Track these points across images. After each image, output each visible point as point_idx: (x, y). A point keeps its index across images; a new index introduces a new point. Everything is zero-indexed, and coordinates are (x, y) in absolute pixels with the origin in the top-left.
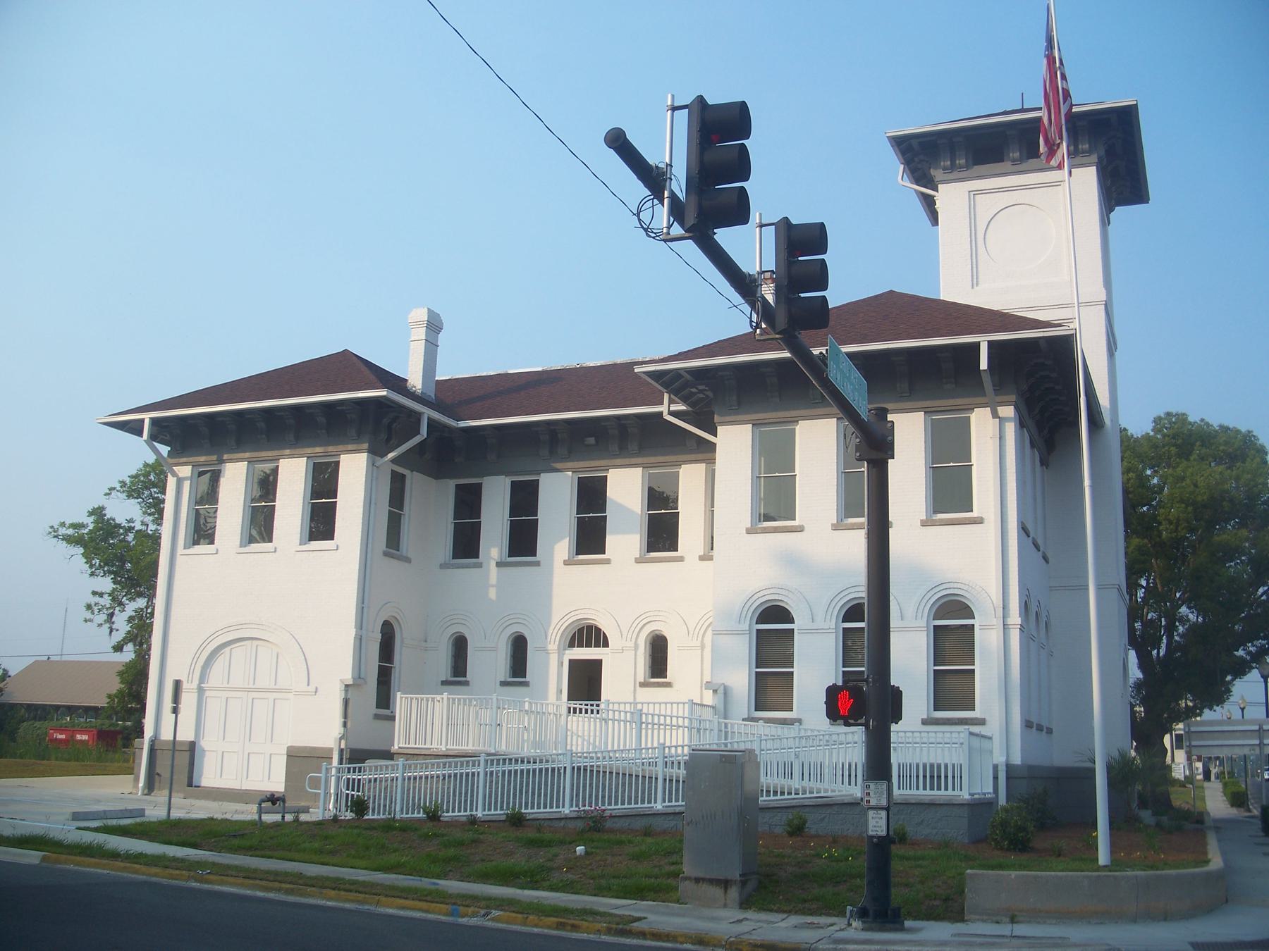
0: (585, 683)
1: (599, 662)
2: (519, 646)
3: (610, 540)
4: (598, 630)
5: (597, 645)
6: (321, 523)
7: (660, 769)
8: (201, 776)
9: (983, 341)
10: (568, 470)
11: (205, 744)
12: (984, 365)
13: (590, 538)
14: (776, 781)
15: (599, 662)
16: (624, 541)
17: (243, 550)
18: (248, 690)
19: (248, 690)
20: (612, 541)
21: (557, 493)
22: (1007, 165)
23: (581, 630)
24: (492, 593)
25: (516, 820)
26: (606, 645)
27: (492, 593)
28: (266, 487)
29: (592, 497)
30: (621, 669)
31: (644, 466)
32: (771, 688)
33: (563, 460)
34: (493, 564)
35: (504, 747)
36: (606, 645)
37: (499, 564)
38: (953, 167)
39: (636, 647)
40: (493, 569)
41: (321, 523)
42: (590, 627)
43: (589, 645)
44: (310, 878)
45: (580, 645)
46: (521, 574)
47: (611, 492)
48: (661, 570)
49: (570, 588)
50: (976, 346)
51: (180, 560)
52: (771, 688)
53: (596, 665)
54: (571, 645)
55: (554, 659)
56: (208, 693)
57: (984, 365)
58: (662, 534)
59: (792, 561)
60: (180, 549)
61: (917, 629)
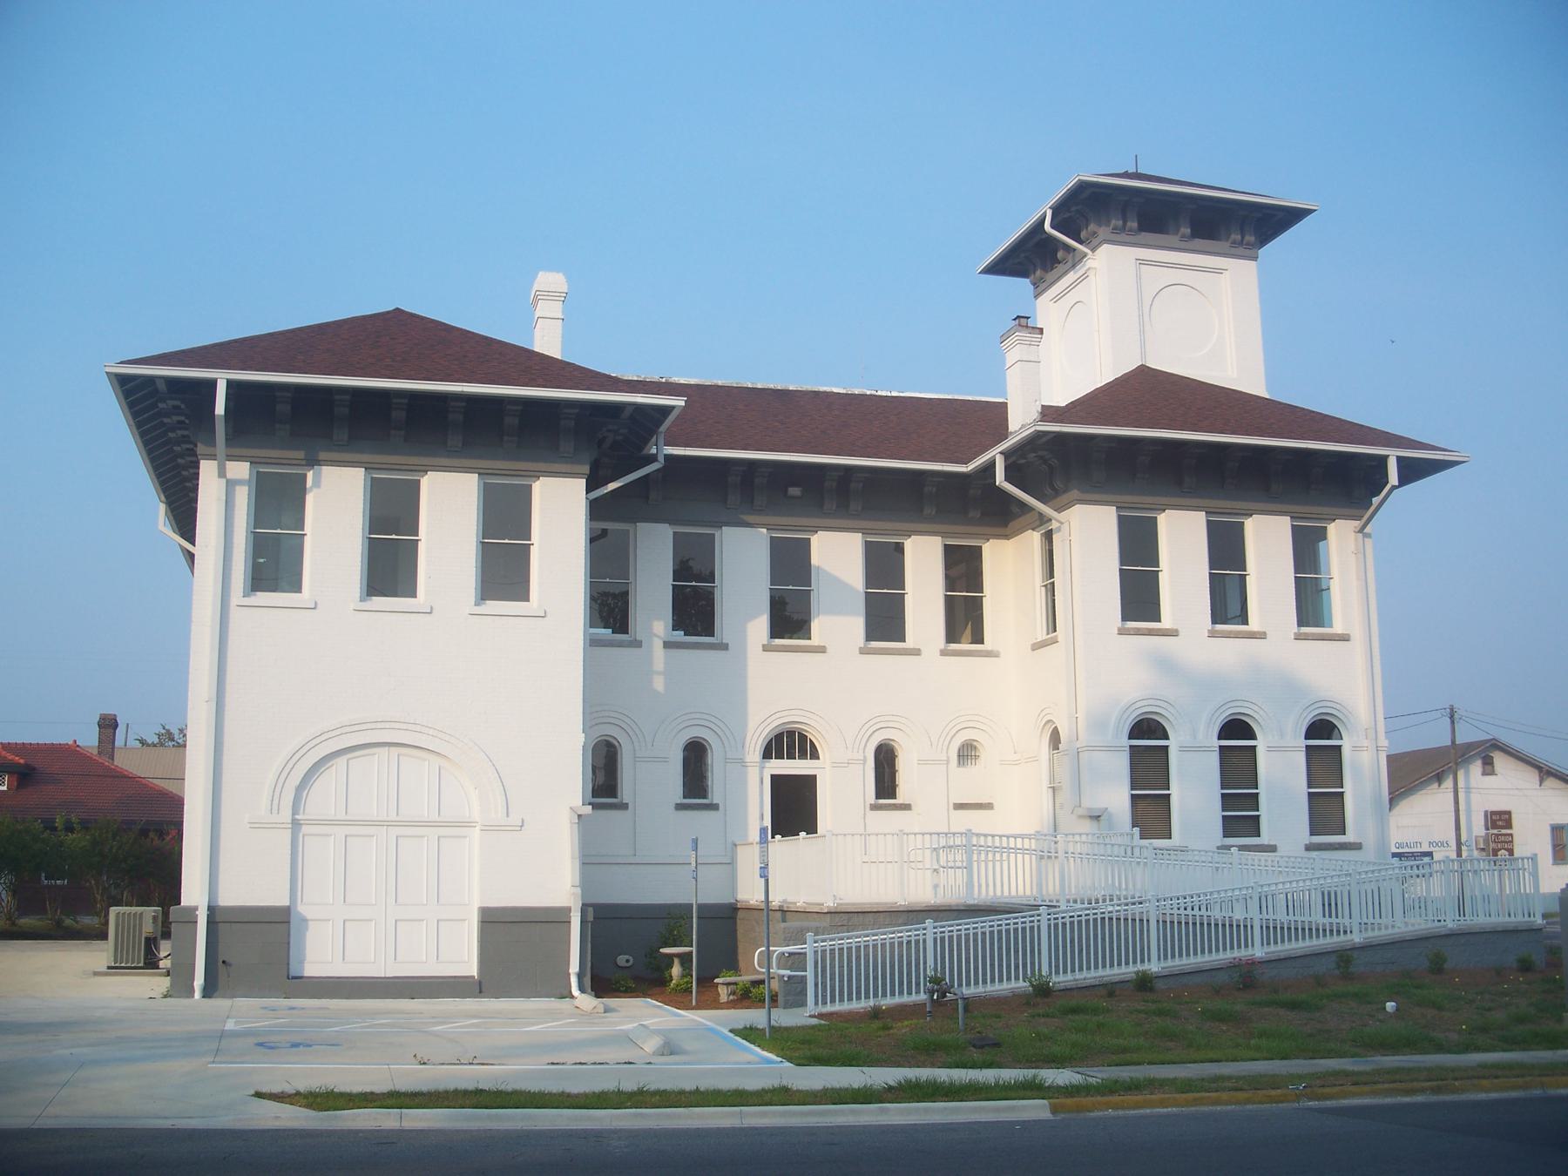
0: (794, 808)
1: (811, 780)
2: (695, 757)
3: (816, 625)
4: (803, 738)
5: (803, 756)
6: (504, 572)
7: (1254, 913)
8: (302, 962)
9: (221, 378)
10: (762, 526)
11: (302, 909)
12: (220, 409)
13: (789, 620)
14: (1306, 919)
15: (811, 780)
16: (838, 625)
17: (479, 610)
18: (389, 824)
19: (389, 824)
20: (820, 626)
21: (743, 558)
22: (1173, 239)
23: (779, 737)
24: (659, 684)
25: (1043, 991)
26: (815, 755)
27: (659, 684)
29: (791, 566)
30: (841, 786)
31: (864, 532)
32: (1152, 813)
33: (760, 512)
34: (658, 645)
35: (1006, 893)
36: (815, 755)
37: (668, 645)
38: (1123, 229)
39: (865, 760)
40: (658, 651)
41: (504, 572)
42: (791, 733)
43: (791, 756)
44: (577, 1096)
45: (780, 756)
46: (698, 660)
47: (816, 559)
48: (885, 665)
49: (770, 683)
50: (212, 384)
51: (236, 615)
52: (1152, 813)
53: (809, 782)
54: (767, 755)
55: (753, 775)
56: (305, 829)
57: (220, 409)
58: (964, 619)
59: (1166, 666)
61: (1294, 749)
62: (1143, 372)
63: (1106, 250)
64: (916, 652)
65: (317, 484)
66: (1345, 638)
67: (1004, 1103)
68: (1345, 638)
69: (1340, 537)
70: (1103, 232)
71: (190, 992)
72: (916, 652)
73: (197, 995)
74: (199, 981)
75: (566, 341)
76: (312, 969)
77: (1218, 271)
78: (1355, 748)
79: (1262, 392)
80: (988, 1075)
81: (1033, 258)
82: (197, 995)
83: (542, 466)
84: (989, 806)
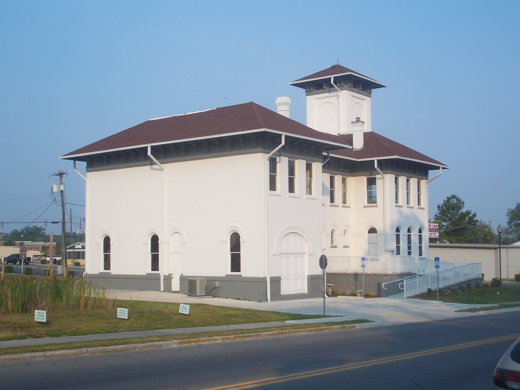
62: (252, 103)
63: (346, 91)
64: (349, 207)
65: (280, 161)
66: (423, 209)
67: (481, 311)
68: (423, 209)
69: (423, 182)
70: (346, 86)
71: (267, 300)
72: (349, 207)
73: (269, 301)
74: (269, 297)
75: (290, 115)
76: (282, 293)
77: (364, 100)
78: (425, 235)
79: (286, 115)
80: (511, 303)
81: (316, 85)
82: (269, 301)
83: (413, 175)
84: (155, 240)
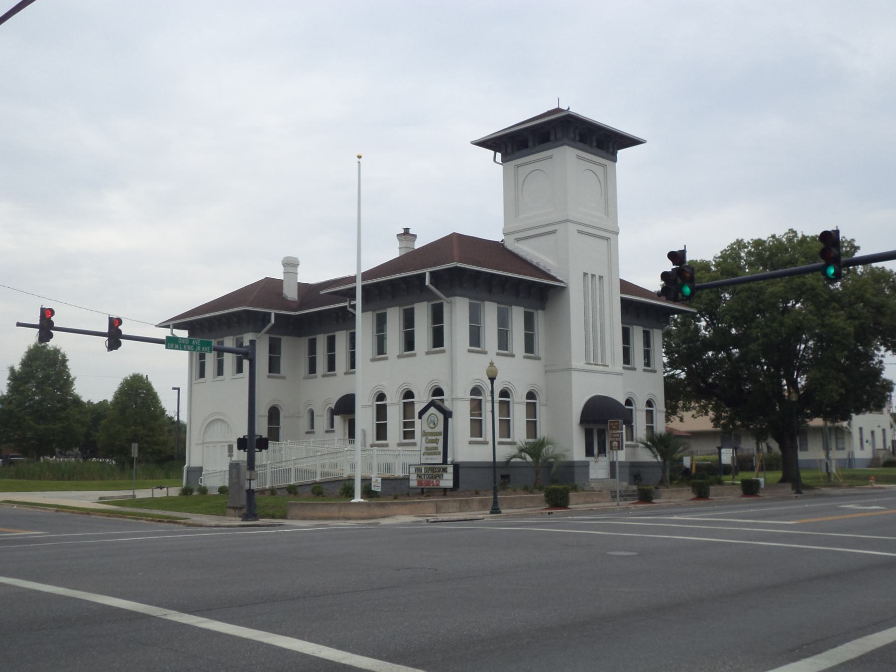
28: (409, 321)
60: (194, 382)
